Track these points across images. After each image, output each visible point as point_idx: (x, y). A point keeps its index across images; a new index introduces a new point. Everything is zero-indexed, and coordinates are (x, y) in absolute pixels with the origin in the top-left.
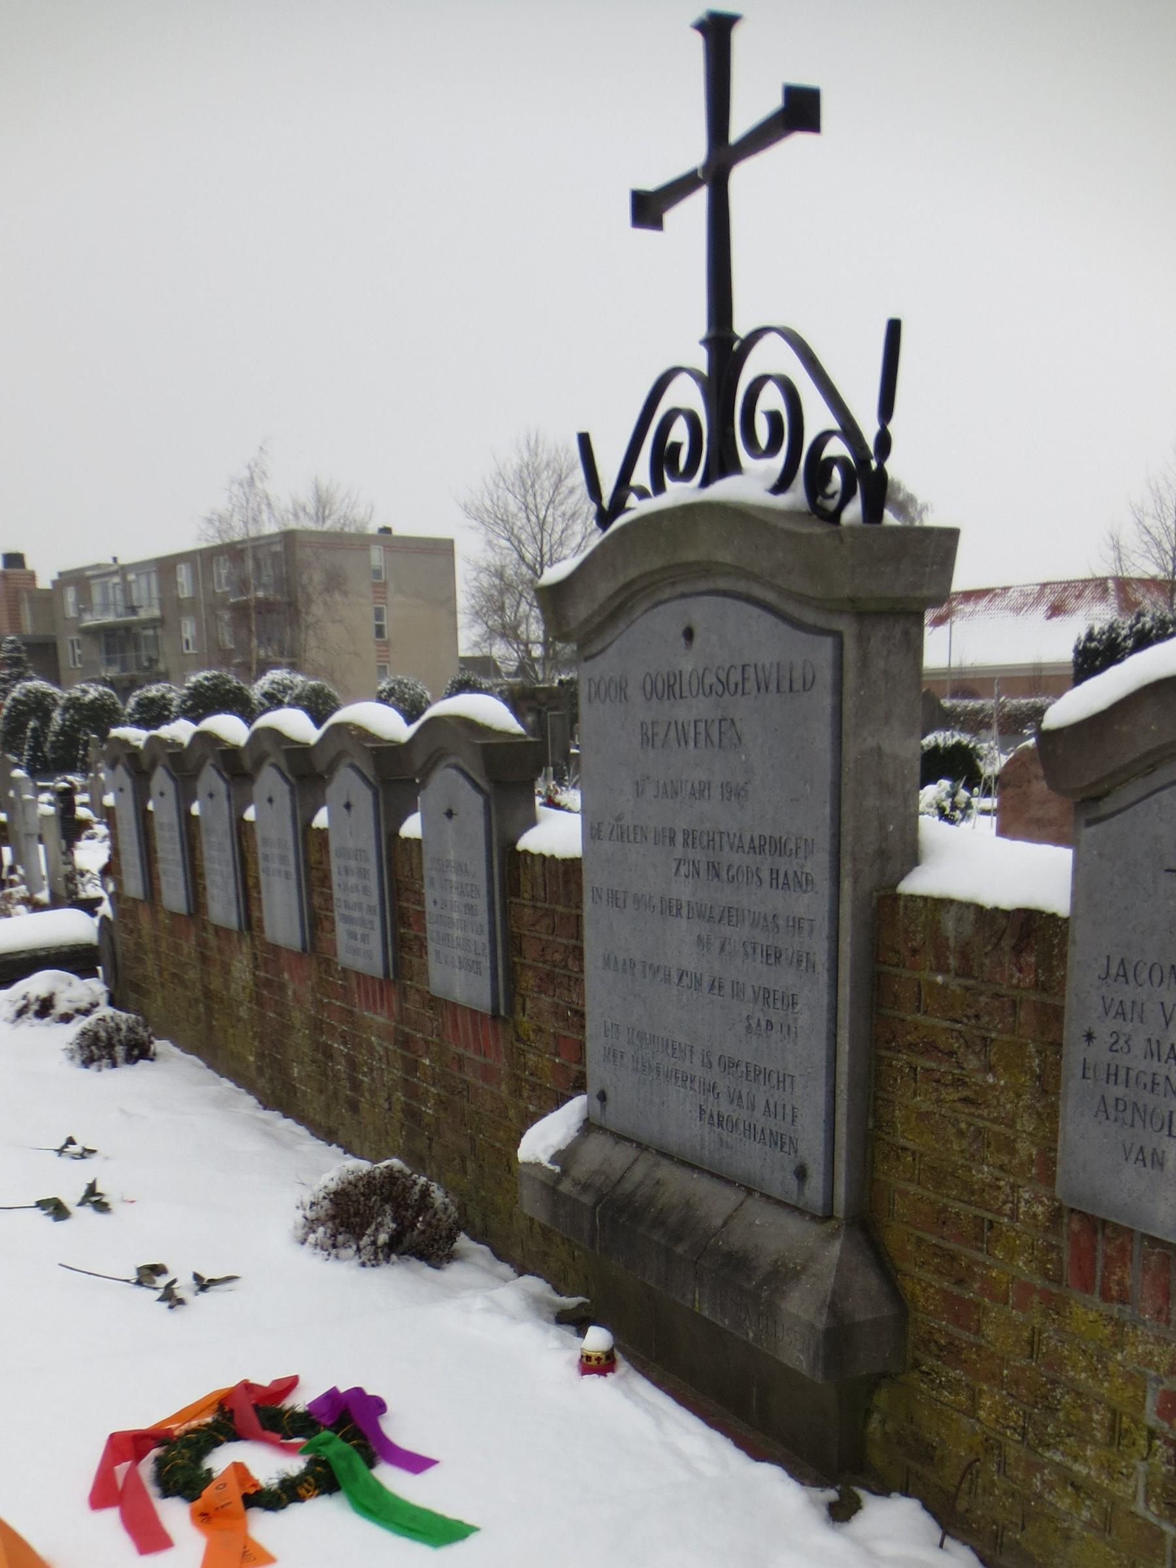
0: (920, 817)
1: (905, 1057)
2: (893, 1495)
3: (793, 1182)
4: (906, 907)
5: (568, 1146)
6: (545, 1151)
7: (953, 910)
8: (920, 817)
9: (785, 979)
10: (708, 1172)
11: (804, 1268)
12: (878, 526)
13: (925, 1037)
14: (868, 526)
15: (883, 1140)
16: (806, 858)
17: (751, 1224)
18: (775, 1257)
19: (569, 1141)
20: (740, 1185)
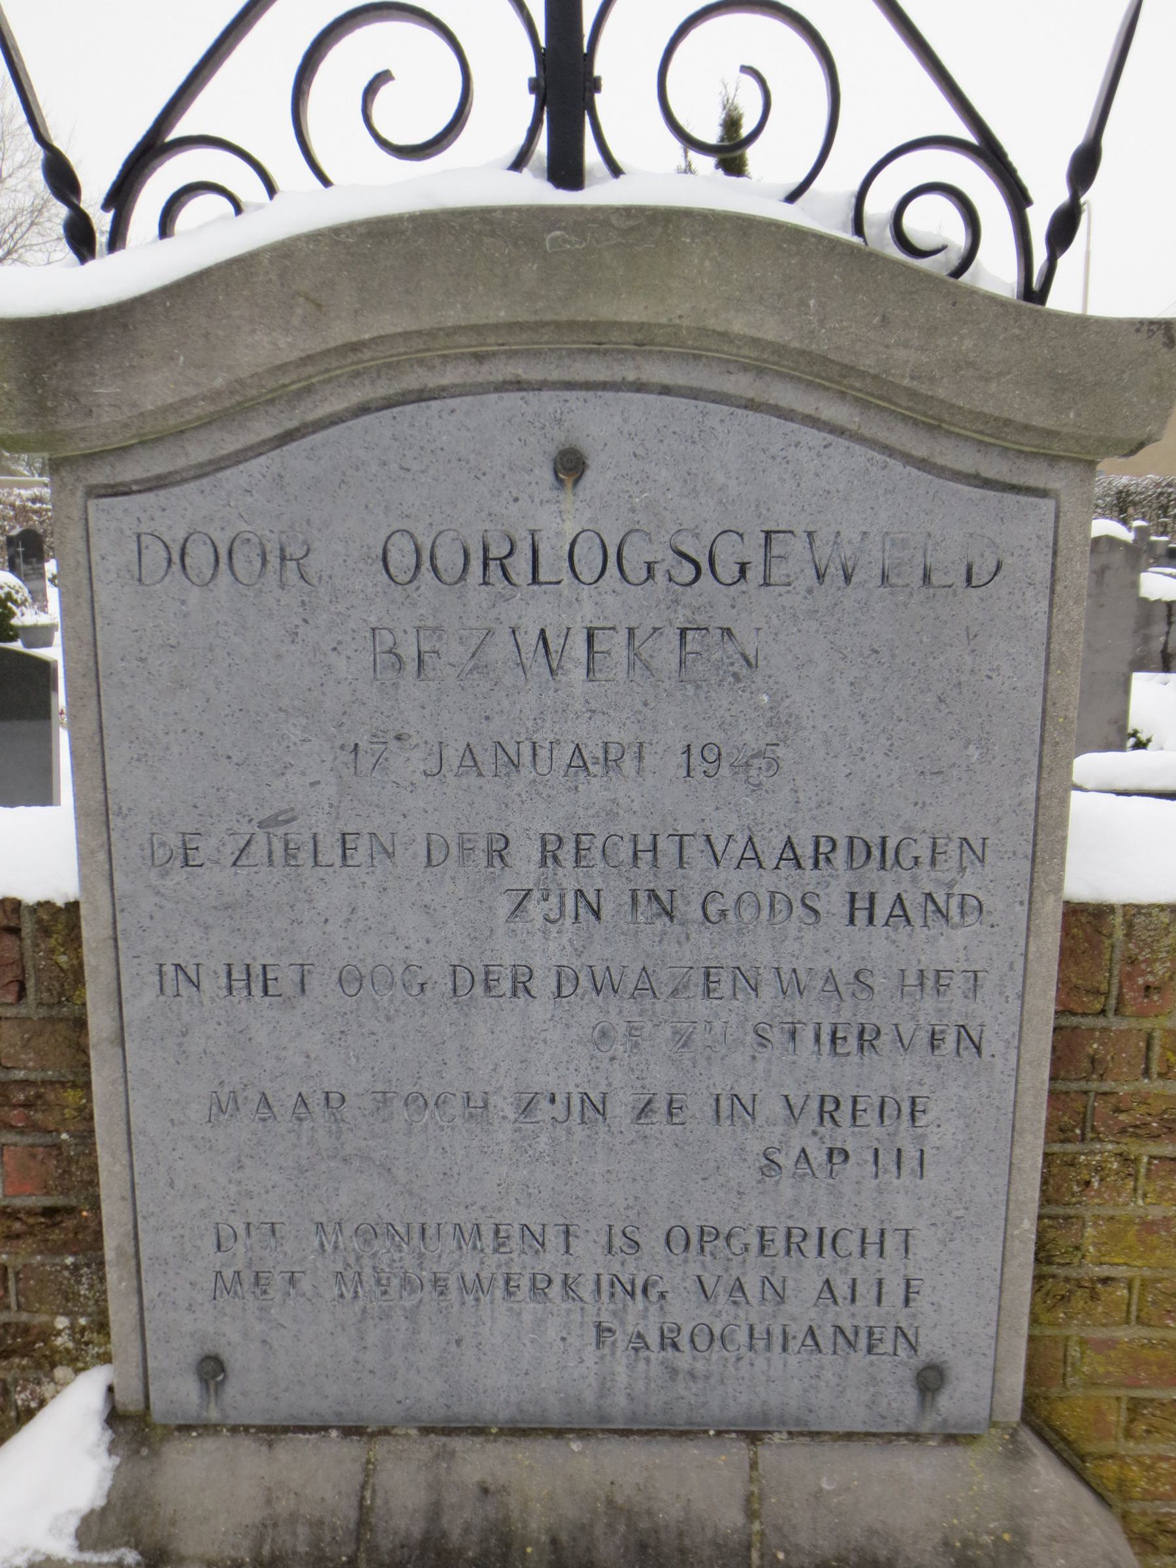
0: (1075, 795)
1: (1110, 1147)
2: (110, 1432)
3: (910, 1398)
4: (1129, 925)
5: (108, 1495)
6: (55, 1530)
7: (85, 1059)
8: (1075, 795)
9: (1006, 1079)
10: (559, 1433)
11: (1022, 1535)
12: (1039, 307)
13: (1164, 1112)
14: (1023, 303)
15: (1054, 1276)
16: (963, 869)
17: (818, 1495)
18: (937, 1537)
19: (107, 1484)
20: (719, 1433)
